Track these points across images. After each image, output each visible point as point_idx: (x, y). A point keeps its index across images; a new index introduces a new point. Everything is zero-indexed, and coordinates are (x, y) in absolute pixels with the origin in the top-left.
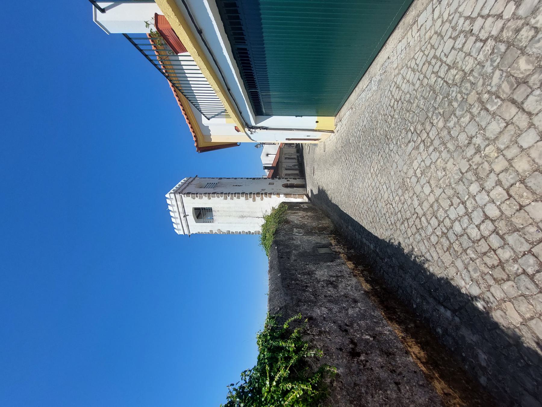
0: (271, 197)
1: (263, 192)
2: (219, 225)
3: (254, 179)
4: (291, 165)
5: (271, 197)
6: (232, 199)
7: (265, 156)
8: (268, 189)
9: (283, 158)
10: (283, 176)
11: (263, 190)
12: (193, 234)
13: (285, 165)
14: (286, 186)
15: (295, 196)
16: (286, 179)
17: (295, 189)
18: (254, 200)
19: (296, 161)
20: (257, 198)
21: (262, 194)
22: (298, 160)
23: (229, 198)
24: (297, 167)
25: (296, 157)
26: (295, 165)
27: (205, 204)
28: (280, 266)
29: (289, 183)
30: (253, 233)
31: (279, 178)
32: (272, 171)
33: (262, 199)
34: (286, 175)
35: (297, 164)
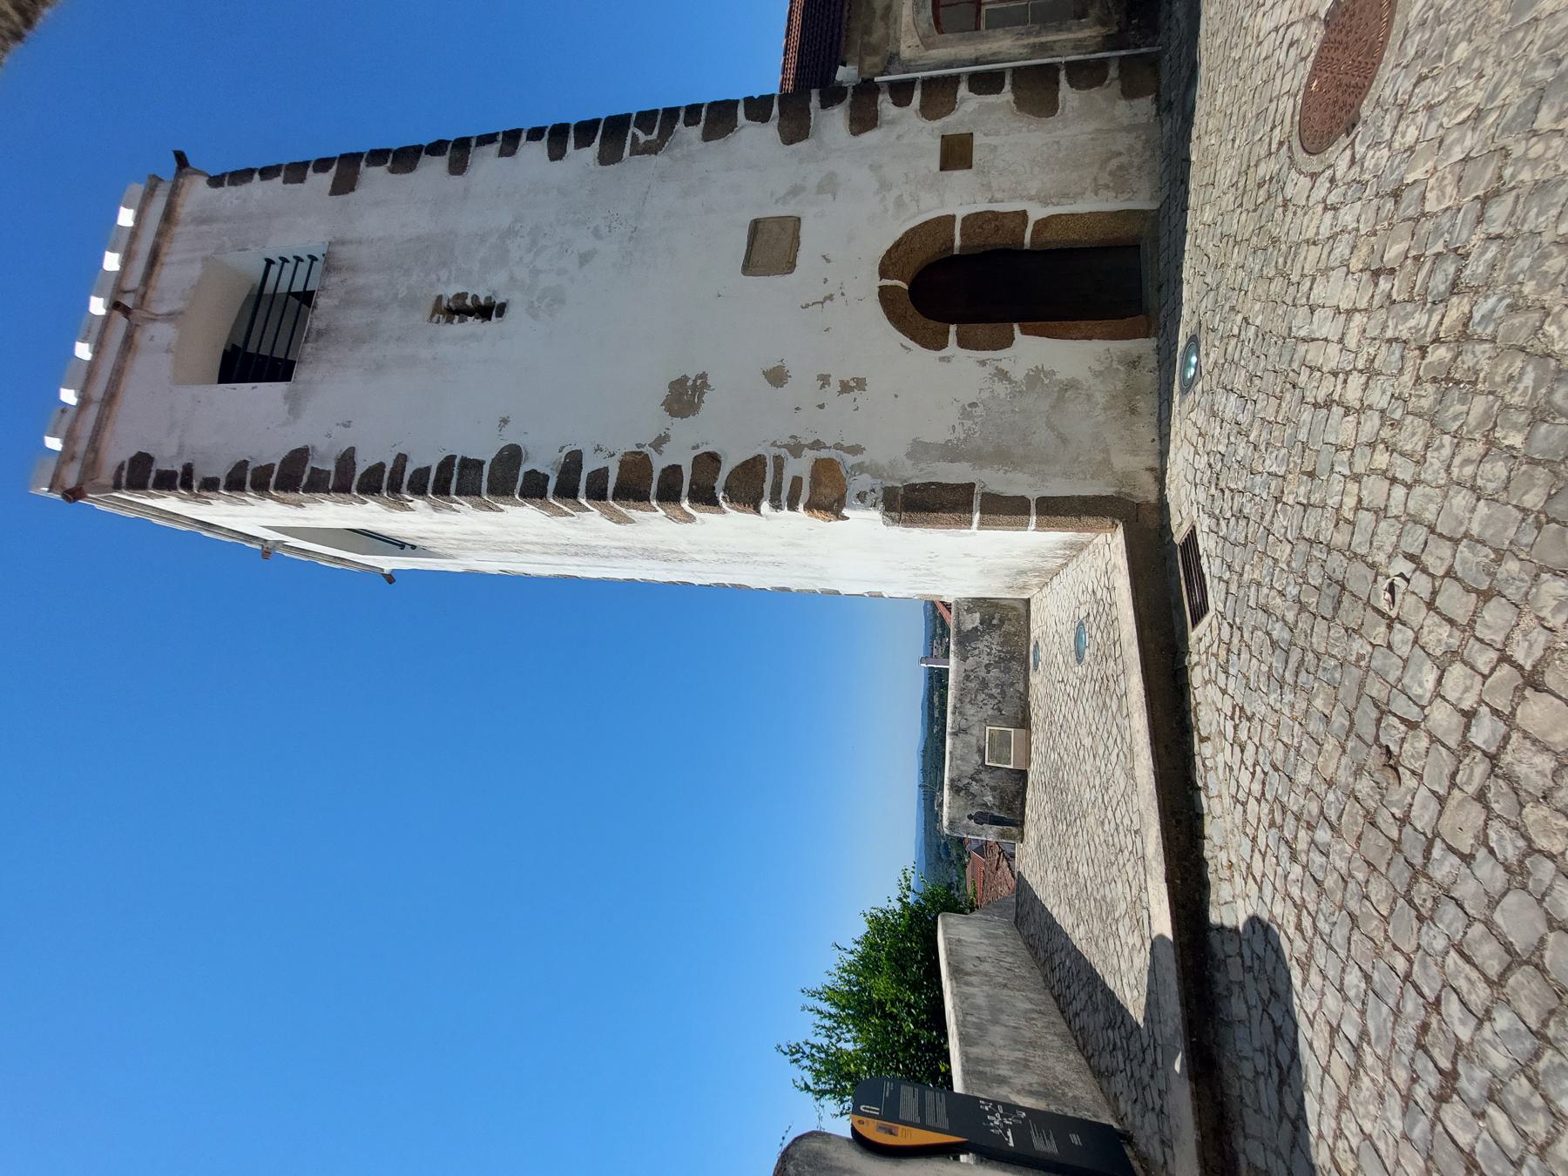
3: (610, 135)
29: (960, 199)
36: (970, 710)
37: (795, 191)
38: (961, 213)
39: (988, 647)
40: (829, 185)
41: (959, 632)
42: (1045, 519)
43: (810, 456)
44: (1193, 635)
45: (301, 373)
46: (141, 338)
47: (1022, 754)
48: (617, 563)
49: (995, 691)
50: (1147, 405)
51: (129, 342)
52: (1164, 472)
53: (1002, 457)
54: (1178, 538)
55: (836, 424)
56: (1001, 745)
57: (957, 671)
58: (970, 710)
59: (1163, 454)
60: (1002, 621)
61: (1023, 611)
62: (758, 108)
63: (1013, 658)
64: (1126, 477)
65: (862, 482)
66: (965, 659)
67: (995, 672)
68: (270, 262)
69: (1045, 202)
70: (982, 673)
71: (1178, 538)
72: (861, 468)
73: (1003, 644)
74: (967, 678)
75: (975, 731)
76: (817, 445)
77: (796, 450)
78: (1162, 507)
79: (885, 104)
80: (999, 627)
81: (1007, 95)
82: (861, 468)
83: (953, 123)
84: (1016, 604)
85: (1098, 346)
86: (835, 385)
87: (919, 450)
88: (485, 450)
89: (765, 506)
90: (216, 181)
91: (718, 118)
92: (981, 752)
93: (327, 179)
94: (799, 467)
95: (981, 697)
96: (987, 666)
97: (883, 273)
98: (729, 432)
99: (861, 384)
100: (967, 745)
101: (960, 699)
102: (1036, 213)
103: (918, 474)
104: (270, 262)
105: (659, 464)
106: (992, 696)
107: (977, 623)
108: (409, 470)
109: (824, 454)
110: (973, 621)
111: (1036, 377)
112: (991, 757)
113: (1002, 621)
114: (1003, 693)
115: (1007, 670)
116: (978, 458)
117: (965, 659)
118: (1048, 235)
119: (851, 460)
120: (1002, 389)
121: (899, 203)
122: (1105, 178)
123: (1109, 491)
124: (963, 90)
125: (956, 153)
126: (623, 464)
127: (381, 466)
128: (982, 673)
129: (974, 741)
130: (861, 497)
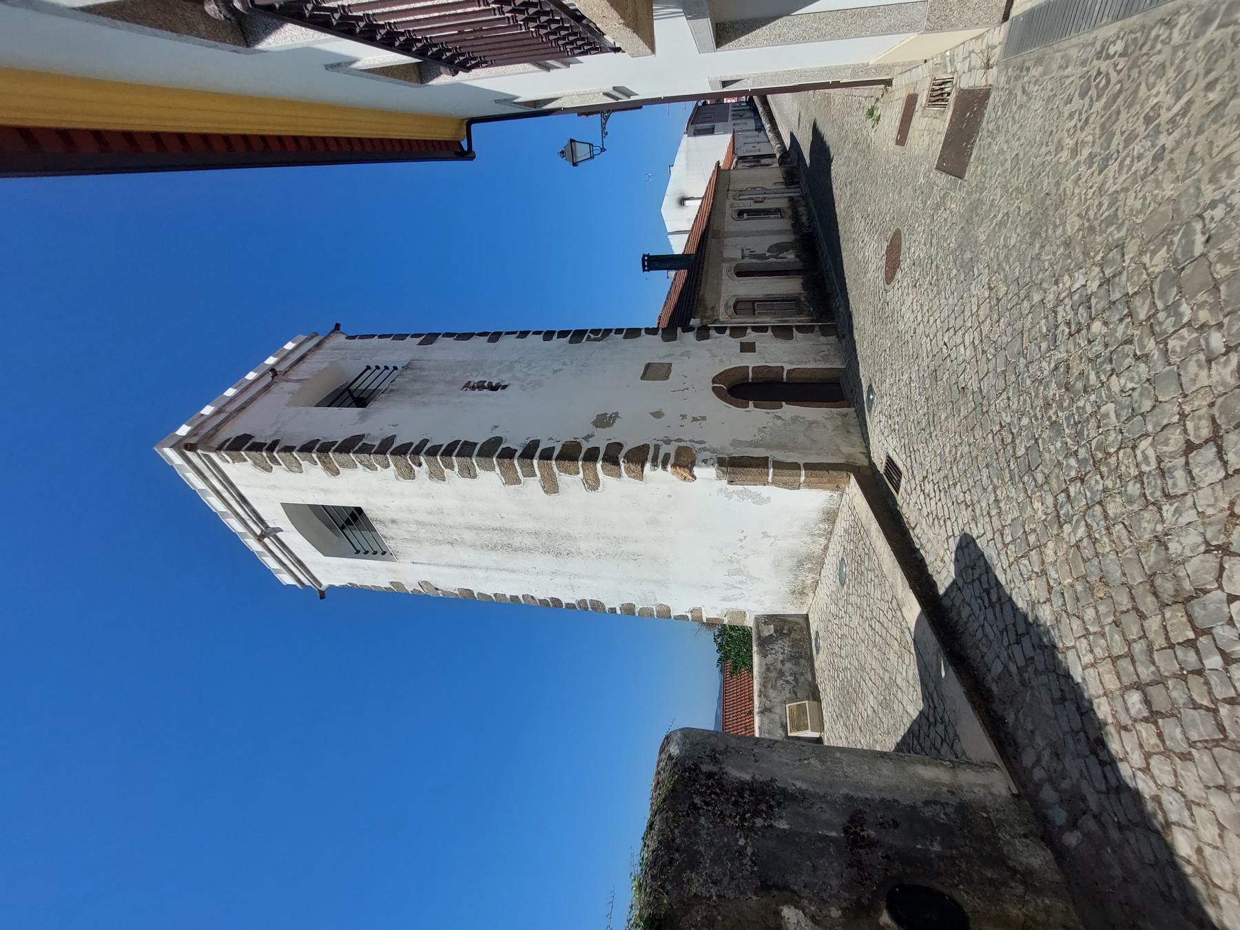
0: (640, 476)
1: (601, 440)
2: (408, 569)
3: (578, 335)
4: (761, 245)
5: (640, 476)
6: (437, 475)
7: (674, 203)
8: (638, 411)
9: (729, 212)
10: (723, 315)
11: (604, 421)
12: (331, 587)
13: (733, 250)
14: (740, 389)
15: (786, 476)
16: (737, 331)
17: (789, 411)
18: (551, 487)
19: (784, 224)
20: (563, 479)
21: (592, 456)
22: (796, 217)
23: (422, 471)
24: (790, 256)
25: (782, 203)
26: (779, 248)
27: (326, 491)
28: (684, 743)
29: (750, 361)
30: (570, 606)
31: (703, 333)
32: (684, 273)
33: (593, 484)
34: (740, 306)
35: (788, 238)
36: (772, 694)
37: (670, 355)
38: (751, 366)
39: (781, 648)
40: (687, 354)
41: (759, 637)
42: (809, 472)
43: (674, 445)
44: (899, 498)
45: (373, 406)
46: (274, 388)
47: (816, 720)
48: (522, 561)
49: (789, 678)
50: (855, 430)
51: (267, 388)
52: (869, 453)
53: (782, 447)
54: (881, 468)
55: (689, 434)
56: (799, 715)
57: (760, 665)
58: (772, 694)
59: (867, 446)
60: (790, 631)
61: (804, 625)
62: (651, 331)
63: (801, 657)
64: (849, 456)
65: (706, 455)
66: (765, 656)
67: (788, 665)
68: (368, 368)
69: (792, 363)
70: (779, 666)
71: (881, 468)
72: (705, 449)
73: (792, 647)
74: (768, 669)
75: (778, 710)
76: (679, 440)
77: (668, 442)
78: (872, 465)
79: (713, 333)
80: (788, 635)
81: (770, 332)
82: (705, 449)
83: (745, 339)
84: (798, 620)
85: (828, 410)
86: (689, 418)
87: (736, 443)
88: (480, 439)
89: (648, 466)
90: (348, 338)
91: (633, 333)
92: (784, 727)
93: (419, 340)
94: (671, 449)
95: (780, 682)
96: (782, 662)
97: (714, 382)
98: (628, 435)
99: (704, 418)
100: (772, 721)
101: (764, 685)
102: (787, 367)
103: (736, 453)
104: (368, 368)
105: (586, 446)
106: (787, 682)
107: (772, 631)
108: (429, 445)
109: (683, 444)
110: (769, 630)
111: (795, 419)
112: (792, 727)
113: (790, 631)
114: (796, 680)
115: (797, 664)
116: (769, 447)
117: (765, 656)
118: (794, 375)
119: (698, 446)
120: (779, 422)
121: (721, 361)
122: (818, 357)
123: (842, 461)
124: (749, 331)
125: (748, 348)
126: (563, 446)
127: (411, 444)
128: (779, 666)
129: (777, 718)
130: (705, 461)
